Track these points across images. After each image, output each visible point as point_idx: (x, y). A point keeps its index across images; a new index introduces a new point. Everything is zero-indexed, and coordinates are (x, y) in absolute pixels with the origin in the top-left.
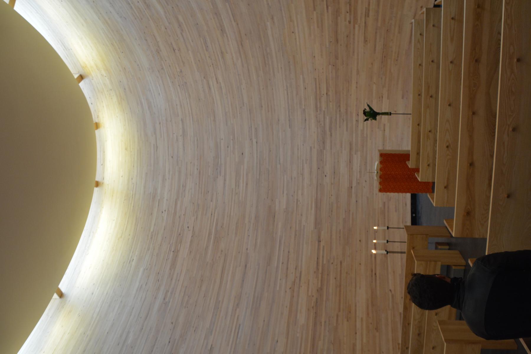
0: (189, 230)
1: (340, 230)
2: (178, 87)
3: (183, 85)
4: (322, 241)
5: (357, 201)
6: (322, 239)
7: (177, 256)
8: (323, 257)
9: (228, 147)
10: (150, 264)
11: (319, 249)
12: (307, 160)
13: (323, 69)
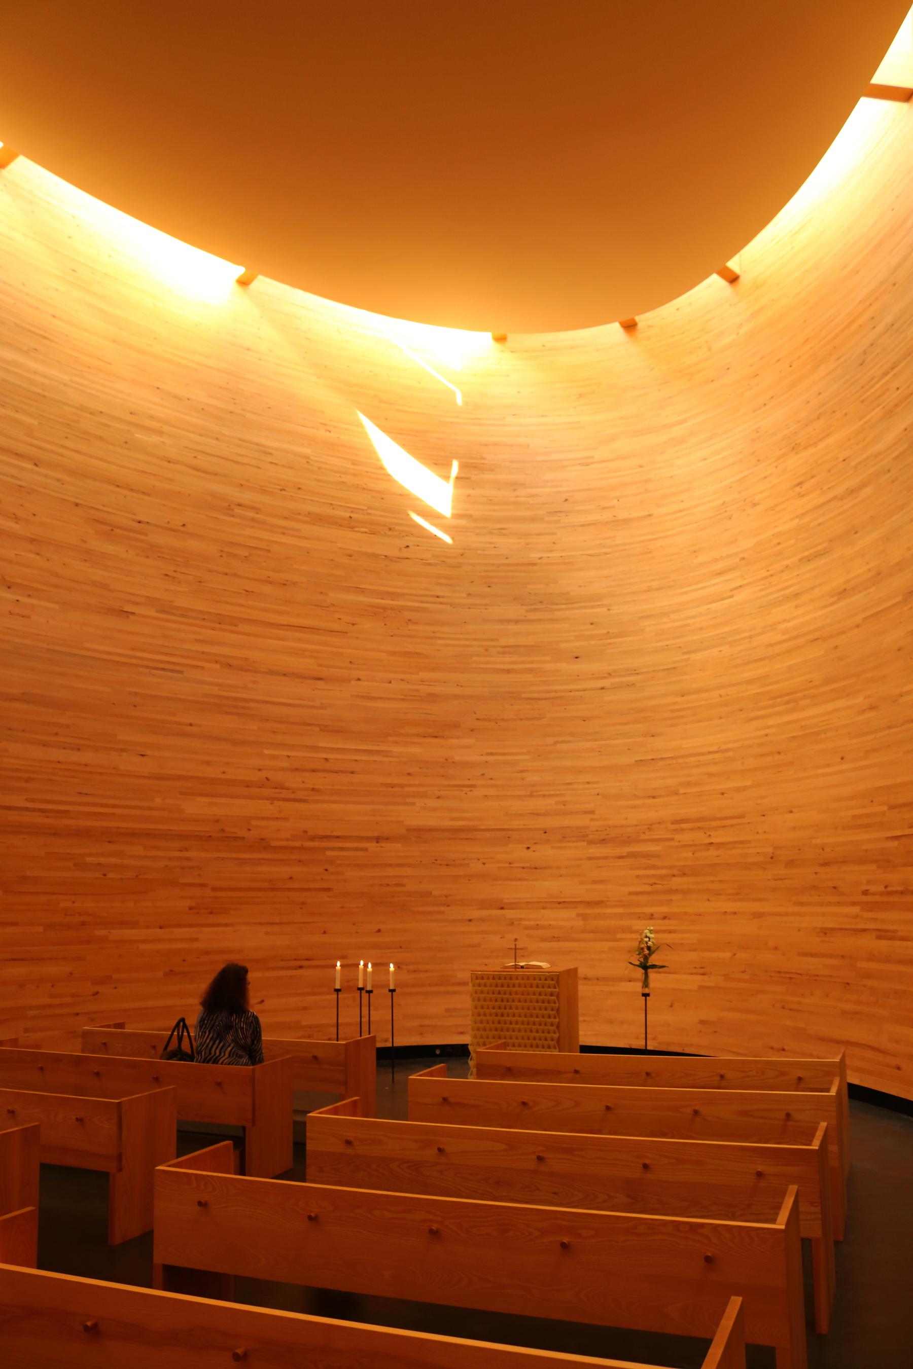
0: (400, 549)
2: (721, 501)
3: (726, 511)
4: (377, 844)
5: (470, 920)
6: (383, 845)
7: (341, 526)
8: (342, 849)
9: (592, 624)
10: (319, 468)
12: (564, 805)
13: (765, 832)
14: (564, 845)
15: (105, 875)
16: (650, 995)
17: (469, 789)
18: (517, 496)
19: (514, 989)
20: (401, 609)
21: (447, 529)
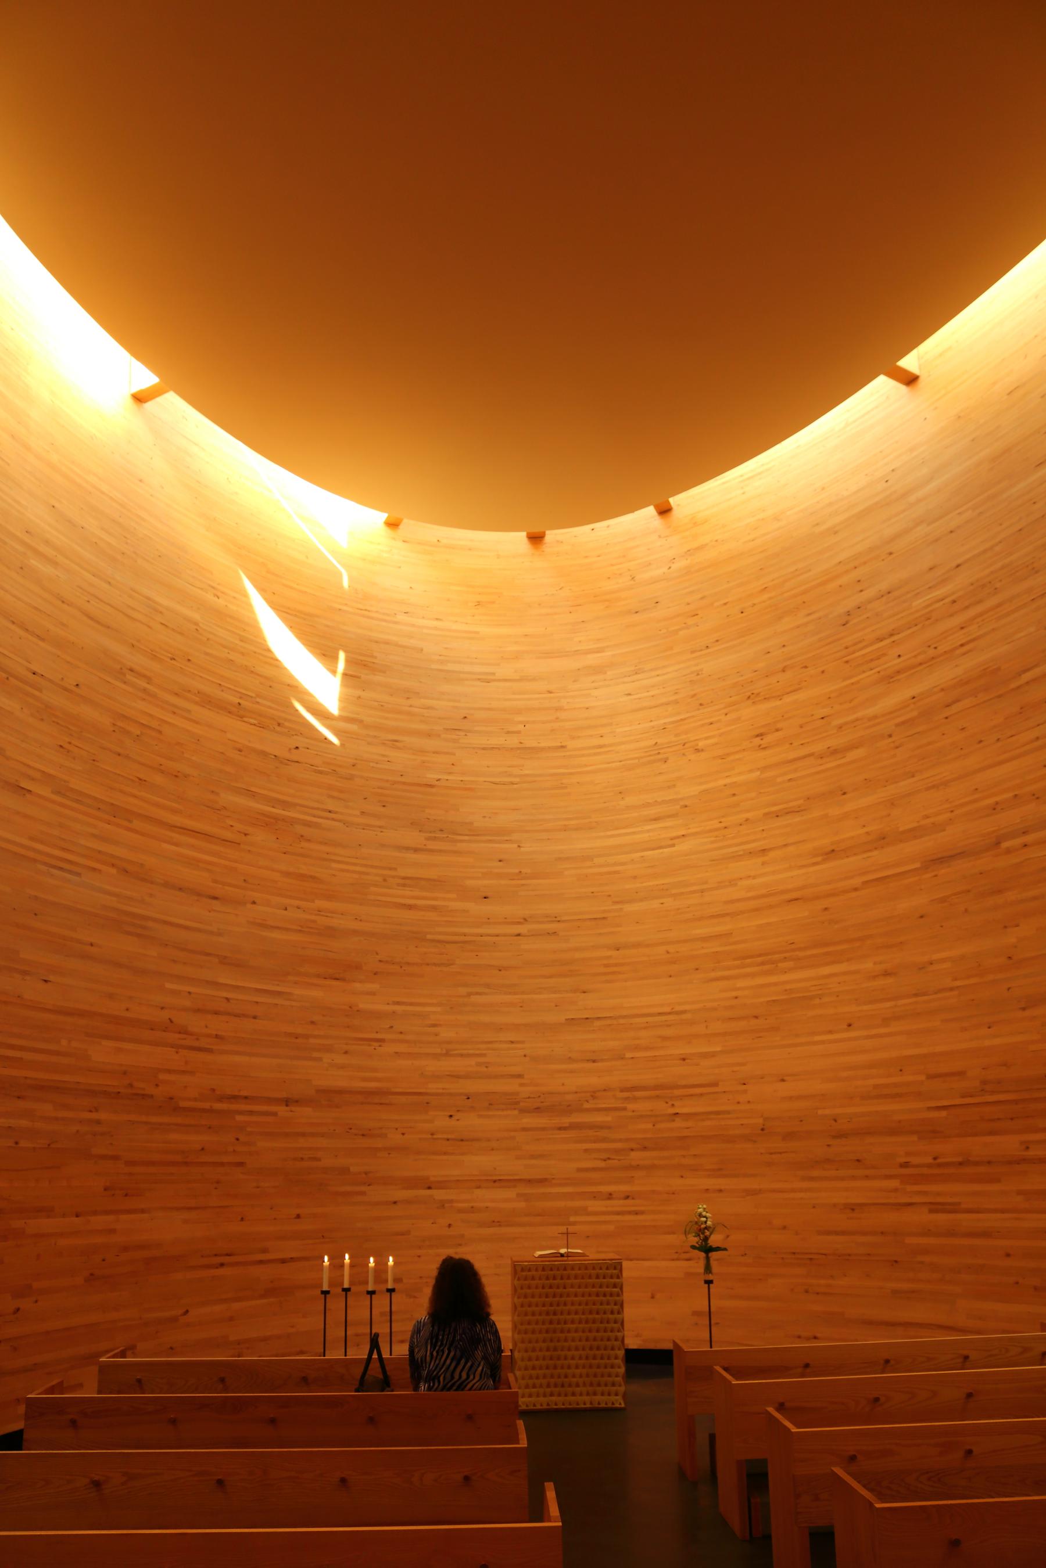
1: (319, 1160)
3: (659, 753)
5: (395, 1203)
6: (293, 1109)
8: (251, 1113)
9: (500, 861)
10: (208, 639)
11: (270, 1101)
12: (487, 1067)
14: (491, 1113)
15: (17, 1143)
16: (714, 1282)
17: (376, 1044)
18: (411, 706)
19: (570, 1281)
20: (292, 822)
21: (337, 732)
